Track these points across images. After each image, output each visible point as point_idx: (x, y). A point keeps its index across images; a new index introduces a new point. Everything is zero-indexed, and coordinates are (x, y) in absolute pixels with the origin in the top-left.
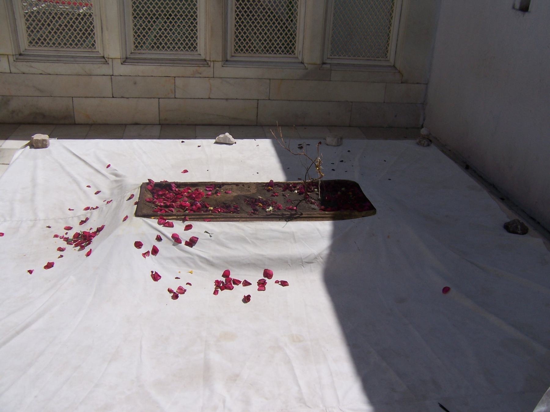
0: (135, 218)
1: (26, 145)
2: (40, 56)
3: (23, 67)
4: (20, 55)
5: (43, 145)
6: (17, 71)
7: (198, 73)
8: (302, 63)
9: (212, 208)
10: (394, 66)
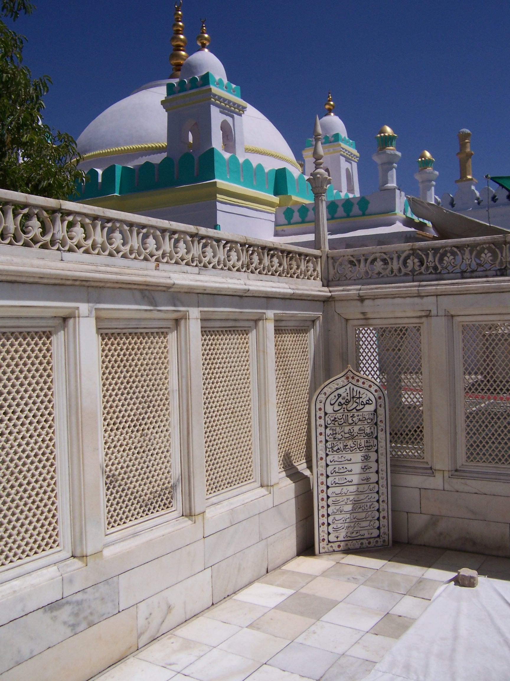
1: (451, 581)
2: (478, 473)
3: (457, 484)
4: (456, 470)
5: (469, 583)
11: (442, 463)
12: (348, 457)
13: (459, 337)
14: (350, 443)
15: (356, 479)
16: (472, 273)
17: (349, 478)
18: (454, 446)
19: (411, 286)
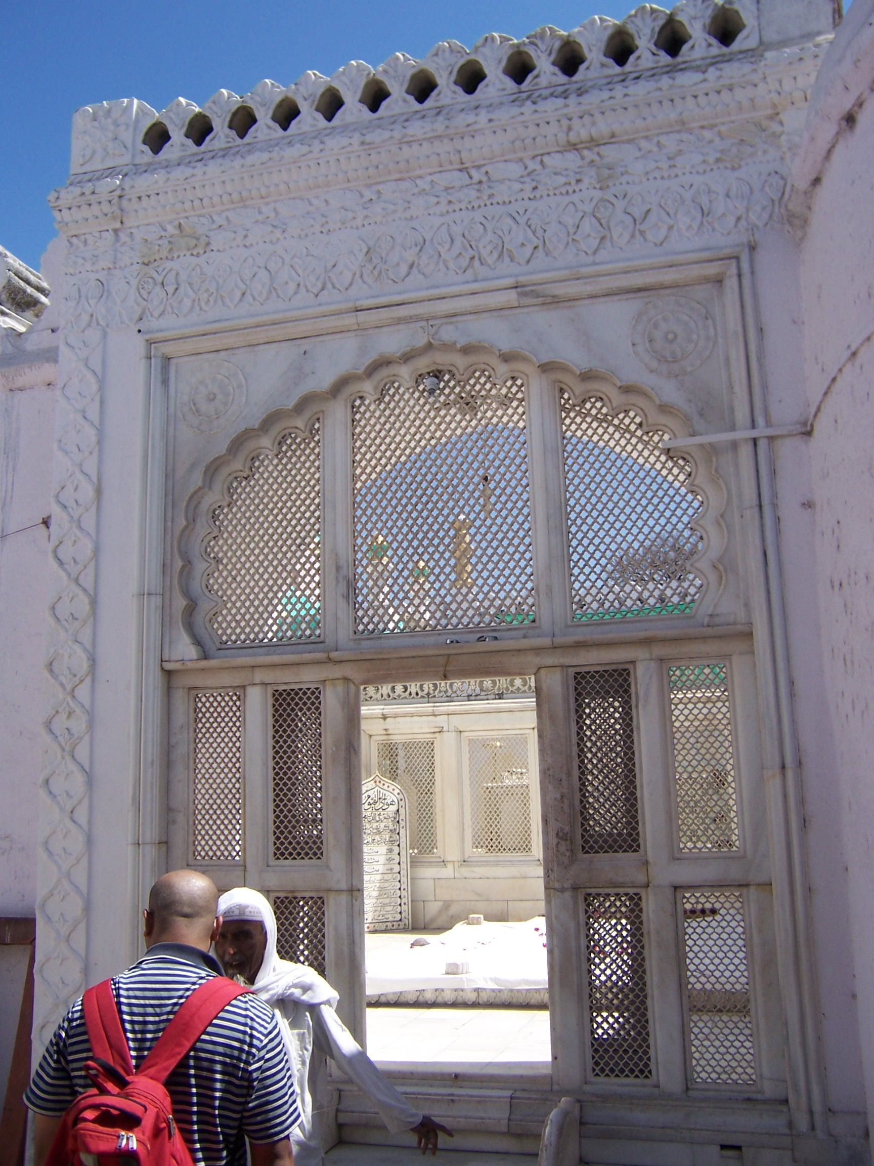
3: (465, 871)
11: (452, 854)
12: (376, 849)
13: (466, 749)
14: (377, 838)
15: (381, 869)
16: (477, 697)
17: (376, 868)
18: (463, 840)
19: (427, 707)
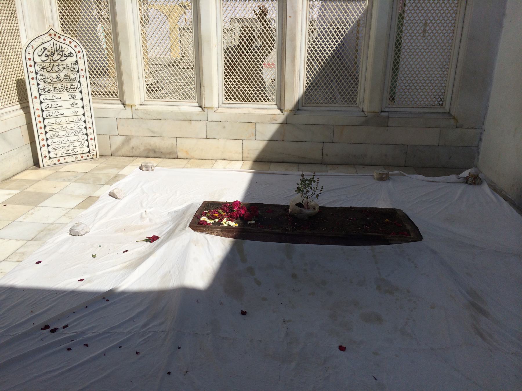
0: (424, 239)
6: (137, 117)
7: (274, 120)
8: (363, 111)
9: (253, 222)
10: (449, 113)
12: (58, 96)
14: (58, 86)
